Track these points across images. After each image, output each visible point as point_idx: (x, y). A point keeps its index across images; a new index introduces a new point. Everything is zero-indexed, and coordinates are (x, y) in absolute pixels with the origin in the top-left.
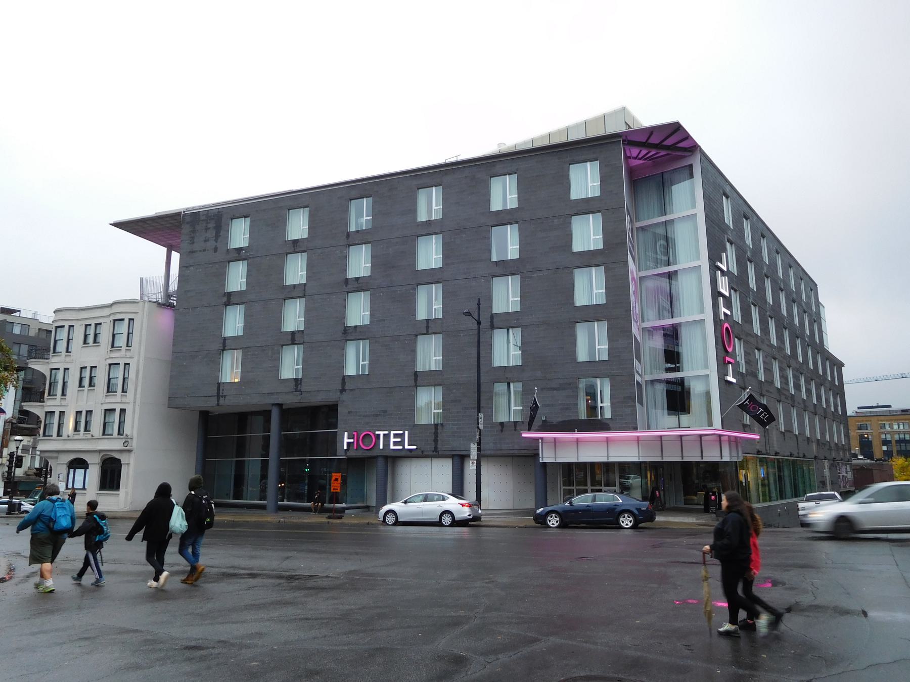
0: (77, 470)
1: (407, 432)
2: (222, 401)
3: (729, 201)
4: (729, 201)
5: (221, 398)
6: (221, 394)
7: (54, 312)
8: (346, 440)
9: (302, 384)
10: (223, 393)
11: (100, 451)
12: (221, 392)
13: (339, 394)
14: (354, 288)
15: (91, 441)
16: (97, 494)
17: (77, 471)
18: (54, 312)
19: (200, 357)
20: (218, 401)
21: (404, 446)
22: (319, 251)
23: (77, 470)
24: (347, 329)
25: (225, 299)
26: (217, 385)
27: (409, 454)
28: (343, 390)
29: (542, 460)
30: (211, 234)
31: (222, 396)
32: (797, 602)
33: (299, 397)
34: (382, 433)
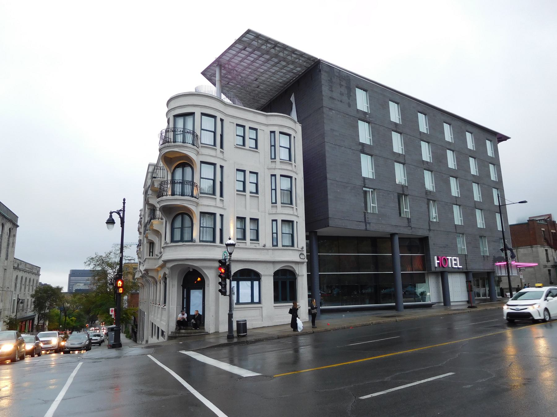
0: (241, 283)
1: (458, 258)
2: (368, 227)
3: (479, 186)
4: (479, 186)
5: (367, 225)
6: (367, 221)
7: (140, 211)
8: (437, 262)
9: (411, 222)
10: (368, 221)
11: (274, 262)
12: (367, 219)
13: (428, 231)
14: (426, 167)
15: (263, 251)
16: (274, 306)
17: (241, 283)
18: (140, 211)
19: (349, 188)
20: (366, 226)
21: (458, 266)
22: (409, 136)
23: (241, 283)
24: (427, 191)
25: (360, 147)
26: (364, 213)
27: (453, 270)
28: (430, 230)
29: (498, 274)
30: (344, 90)
31: (368, 223)
32: (91, 288)
33: (411, 231)
34: (449, 258)
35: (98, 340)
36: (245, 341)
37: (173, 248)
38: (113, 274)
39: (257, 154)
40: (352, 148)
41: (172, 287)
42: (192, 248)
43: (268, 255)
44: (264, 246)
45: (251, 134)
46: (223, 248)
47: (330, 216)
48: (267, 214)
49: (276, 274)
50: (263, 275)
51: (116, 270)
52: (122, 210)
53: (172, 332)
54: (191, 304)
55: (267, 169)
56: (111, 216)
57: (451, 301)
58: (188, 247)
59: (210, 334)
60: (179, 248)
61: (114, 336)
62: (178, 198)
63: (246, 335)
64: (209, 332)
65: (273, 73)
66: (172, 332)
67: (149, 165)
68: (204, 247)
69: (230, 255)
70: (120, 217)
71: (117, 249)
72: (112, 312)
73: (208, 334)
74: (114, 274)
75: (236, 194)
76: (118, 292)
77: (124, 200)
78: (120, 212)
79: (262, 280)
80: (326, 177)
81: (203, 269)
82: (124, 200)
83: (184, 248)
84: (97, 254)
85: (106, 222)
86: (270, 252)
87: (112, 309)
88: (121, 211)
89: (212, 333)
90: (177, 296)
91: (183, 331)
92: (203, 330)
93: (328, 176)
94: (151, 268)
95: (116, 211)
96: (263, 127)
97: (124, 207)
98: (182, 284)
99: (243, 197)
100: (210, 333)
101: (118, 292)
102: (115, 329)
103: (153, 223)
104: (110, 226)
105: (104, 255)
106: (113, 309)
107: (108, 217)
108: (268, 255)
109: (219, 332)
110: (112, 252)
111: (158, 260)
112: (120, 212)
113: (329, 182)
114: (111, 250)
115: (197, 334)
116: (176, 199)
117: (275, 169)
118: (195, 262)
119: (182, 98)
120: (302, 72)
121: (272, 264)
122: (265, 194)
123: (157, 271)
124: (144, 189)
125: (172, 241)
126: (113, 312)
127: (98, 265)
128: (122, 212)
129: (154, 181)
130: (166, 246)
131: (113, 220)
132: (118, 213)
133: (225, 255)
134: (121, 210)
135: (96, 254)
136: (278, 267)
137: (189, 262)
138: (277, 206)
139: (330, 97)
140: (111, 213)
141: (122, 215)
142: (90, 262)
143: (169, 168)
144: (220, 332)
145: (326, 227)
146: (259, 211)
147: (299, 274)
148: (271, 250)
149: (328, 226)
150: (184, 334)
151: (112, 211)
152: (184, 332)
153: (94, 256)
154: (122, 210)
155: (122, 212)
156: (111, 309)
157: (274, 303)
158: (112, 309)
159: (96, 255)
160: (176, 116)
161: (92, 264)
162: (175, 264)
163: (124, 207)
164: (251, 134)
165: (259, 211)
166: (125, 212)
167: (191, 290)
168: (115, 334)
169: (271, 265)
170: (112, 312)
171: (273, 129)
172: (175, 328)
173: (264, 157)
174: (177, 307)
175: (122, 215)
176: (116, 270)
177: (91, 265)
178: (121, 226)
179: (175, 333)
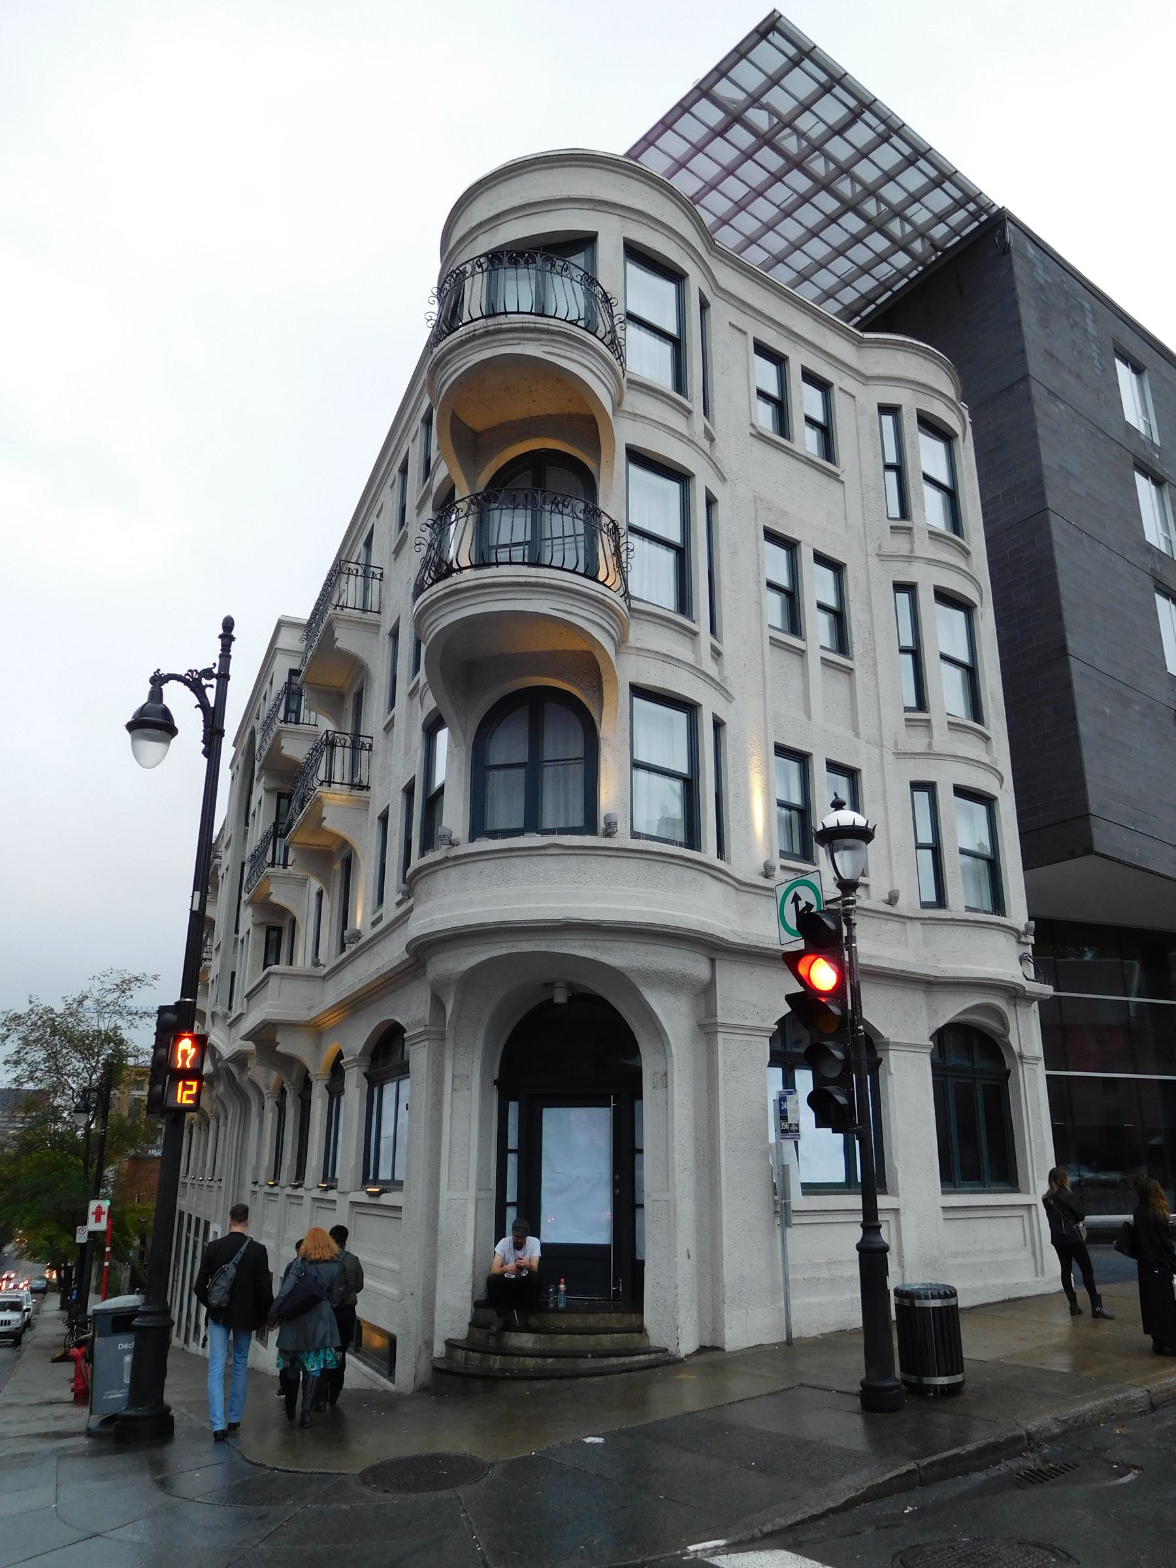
11: (930, 985)
35: (13, 1326)
36: (1019, 1439)
37: (489, 866)
38: (86, 1075)
39: (834, 485)
40: (1128, 557)
41: (454, 1090)
42: (594, 865)
43: (907, 946)
44: (892, 899)
45: (807, 401)
46: (730, 888)
47: (1093, 808)
48: (889, 757)
49: (941, 1036)
50: (898, 1044)
51: (98, 1062)
52: (216, 671)
53: (450, 1344)
54: (544, 1185)
55: (876, 559)
56: (156, 695)
57: (878, 1208)
58: (572, 862)
59: (682, 1361)
60: (520, 866)
61: (128, 1359)
62: (547, 581)
63: (961, 1384)
64: (672, 1349)
65: (798, 272)
66: (450, 1344)
67: (280, 624)
68: (657, 867)
69: (845, 894)
70: (203, 705)
71: (108, 987)
72: (98, 1220)
73: (666, 1362)
74: (91, 1077)
75: (767, 640)
76: (170, 1103)
77: (228, 624)
78: (204, 682)
79: (892, 1069)
80: (1064, 647)
81: (641, 989)
82: (228, 624)
83: (549, 865)
84: (36, 1002)
85: (129, 719)
86: (916, 930)
87: (99, 1207)
88: (209, 678)
89: (687, 1356)
90: (480, 1136)
91: (525, 1340)
92: (636, 1335)
93: (1072, 643)
94: (292, 1018)
95: (182, 672)
96: (851, 385)
97: (225, 656)
98: (496, 1077)
99: (795, 661)
100: (682, 1355)
101: (170, 1103)
102: (136, 1322)
103: (325, 801)
104: (151, 748)
105: (59, 1008)
106: (105, 1204)
107: (141, 697)
108: (907, 946)
109: (724, 1350)
110: (89, 995)
111: (320, 982)
112: (204, 682)
113: (1075, 666)
114: (86, 990)
115: (614, 1361)
116: (536, 585)
117: (910, 558)
118: (609, 945)
119: (525, 176)
120: (912, 275)
121: (922, 995)
122: (875, 665)
123: (315, 1030)
124: (234, 749)
125: (479, 828)
126: (104, 1218)
127: (36, 1041)
128: (214, 682)
129: (335, 624)
130: (446, 859)
131: (166, 713)
132: (194, 683)
133: (796, 899)
134: (207, 673)
135: (31, 1002)
136: (951, 1009)
137: (577, 944)
138: (929, 721)
139: (1046, 351)
140: (158, 680)
141: (211, 694)
142: (9, 1030)
143: (466, 476)
144: (730, 1346)
145: (1072, 855)
146: (857, 735)
147: (1026, 1054)
148: (918, 924)
149: (1089, 850)
150: (539, 1360)
151: (165, 671)
152: (530, 1345)
153: (22, 1009)
154: (216, 671)
155: (214, 682)
156: (93, 1205)
157: (943, 1193)
158: (99, 1207)
159: (31, 1006)
160: (498, 259)
161: (14, 1037)
162: (494, 954)
163: (225, 656)
164: (807, 401)
165: (857, 735)
166: (231, 661)
167: (546, 1111)
168: (137, 1353)
169: (916, 999)
170: (98, 1220)
171: (892, 396)
172: (468, 1318)
173: (863, 507)
174: (477, 1201)
175: (211, 694)
176: (98, 1062)
177: (10, 1039)
178: (206, 753)
179: (469, 1345)
